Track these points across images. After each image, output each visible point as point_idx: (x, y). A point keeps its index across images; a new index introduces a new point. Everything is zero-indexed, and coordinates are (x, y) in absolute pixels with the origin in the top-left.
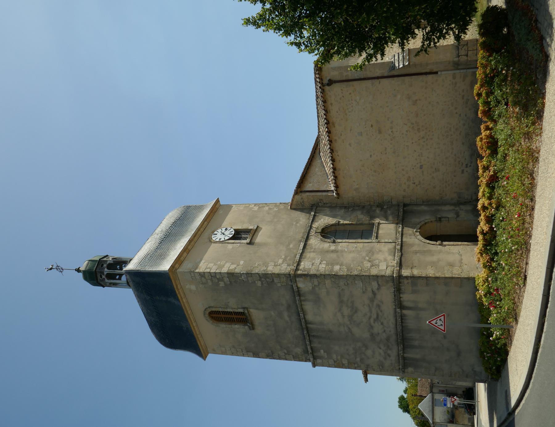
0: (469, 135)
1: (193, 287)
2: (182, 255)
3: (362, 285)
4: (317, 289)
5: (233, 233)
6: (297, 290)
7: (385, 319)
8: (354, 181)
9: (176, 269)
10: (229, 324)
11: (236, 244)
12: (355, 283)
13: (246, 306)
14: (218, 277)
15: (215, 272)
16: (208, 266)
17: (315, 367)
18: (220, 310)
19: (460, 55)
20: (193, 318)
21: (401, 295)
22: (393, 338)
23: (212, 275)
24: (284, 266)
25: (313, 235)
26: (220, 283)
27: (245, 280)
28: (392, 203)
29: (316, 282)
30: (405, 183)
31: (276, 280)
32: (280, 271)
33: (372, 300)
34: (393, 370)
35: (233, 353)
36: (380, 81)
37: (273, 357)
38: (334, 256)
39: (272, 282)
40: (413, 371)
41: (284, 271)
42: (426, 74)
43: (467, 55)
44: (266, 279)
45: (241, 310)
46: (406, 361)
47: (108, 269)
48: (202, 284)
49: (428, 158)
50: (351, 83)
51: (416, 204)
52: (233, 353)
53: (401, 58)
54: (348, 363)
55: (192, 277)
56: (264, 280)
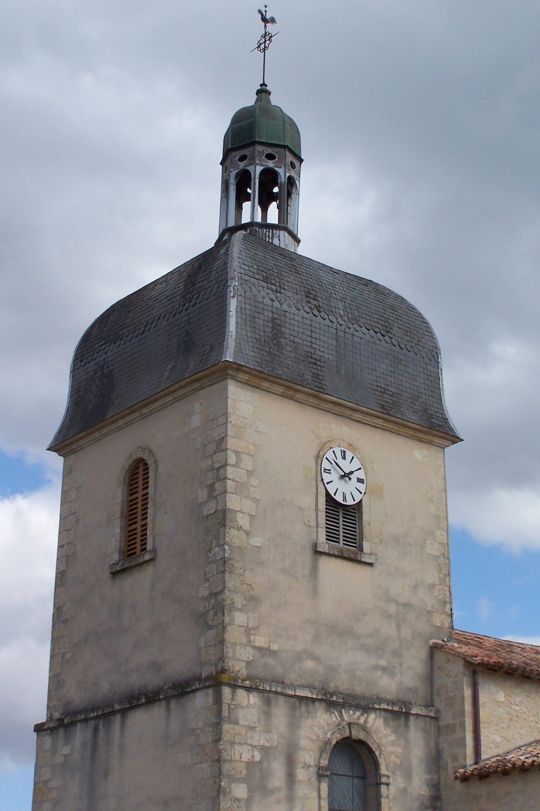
5: (350, 502)
9: (234, 378)
10: (122, 513)
11: (314, 516)
14: (217, 485)
15: (226, 478)
17: (35, 731)
18: (151, 490)
24: (246, 654)
25: (343, 720)
26: (206, 490)
27: (211, 554)
29: (207, 738)
31: (210, 634)
32: (232, 644)
41: (230, 654)
44: (212, 609)
45: (149, 546)
47: (263, 173)
52: (64, 519)
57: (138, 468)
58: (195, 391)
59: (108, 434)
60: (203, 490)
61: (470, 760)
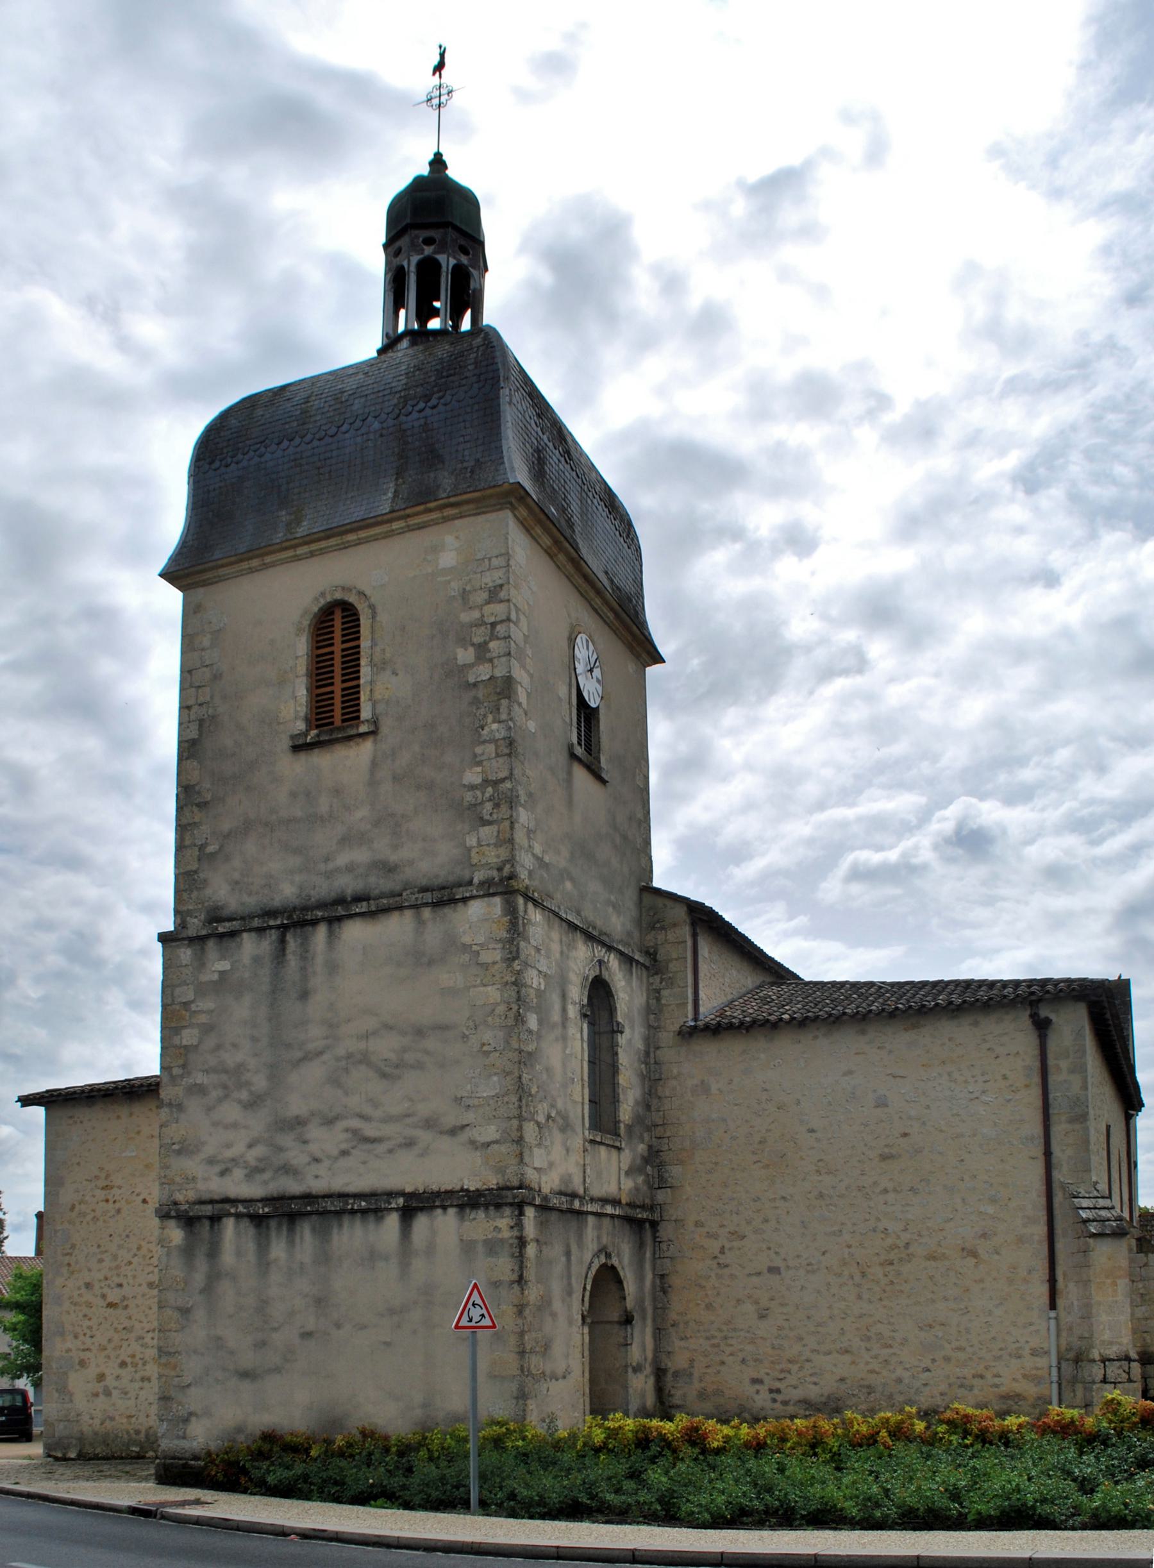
0: (869, 1394)
1: (448, 559)
2: (548, 533)
3: (485, 1095)
4: (466, 957)
6: (457, 897)
7: (364, 1163)
8: (731, 1082)
12: (490, 1076)
13: (384, 730)
16: (522, 617)
18: (365, 644)
19: (1107, 1363)
20: (329, 547)
21: (452, 1211)
22: (294, 1187)
23: (498, 627)
25: (594, 956)
26: (471, 650)
28: (659, 1188)
29: (493, 955)
30: (722, 1226)
33: (429, 1124)
34: (169, 1184)
35: (190, 672)
36: (1036, 1158)
37: (186, 805)
38: (556, 1017)
39: (481, 819)
40: (173, 1244)
42: (1052, 1281)
43: (1104, 1381)
45: (366, 713)
46: (207, 1223)
48: (464, 589)
49: (803, 1288)
50: (1036, 1079)
51: (657, 1256)
53: (1103, 1213)
54: (186, 1047)
55: (486, 561)
56: (487, 795)
57: (332, 613)
58: (446, 519)
59: (273, 565)
60: (466, 650)
61: (690, 1015)
